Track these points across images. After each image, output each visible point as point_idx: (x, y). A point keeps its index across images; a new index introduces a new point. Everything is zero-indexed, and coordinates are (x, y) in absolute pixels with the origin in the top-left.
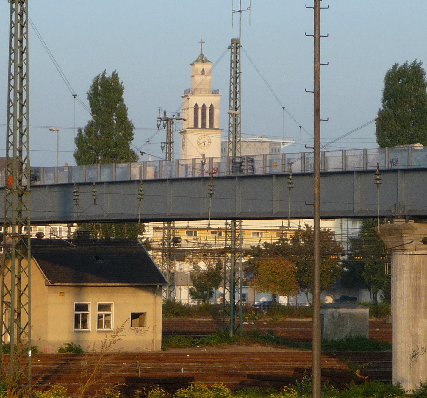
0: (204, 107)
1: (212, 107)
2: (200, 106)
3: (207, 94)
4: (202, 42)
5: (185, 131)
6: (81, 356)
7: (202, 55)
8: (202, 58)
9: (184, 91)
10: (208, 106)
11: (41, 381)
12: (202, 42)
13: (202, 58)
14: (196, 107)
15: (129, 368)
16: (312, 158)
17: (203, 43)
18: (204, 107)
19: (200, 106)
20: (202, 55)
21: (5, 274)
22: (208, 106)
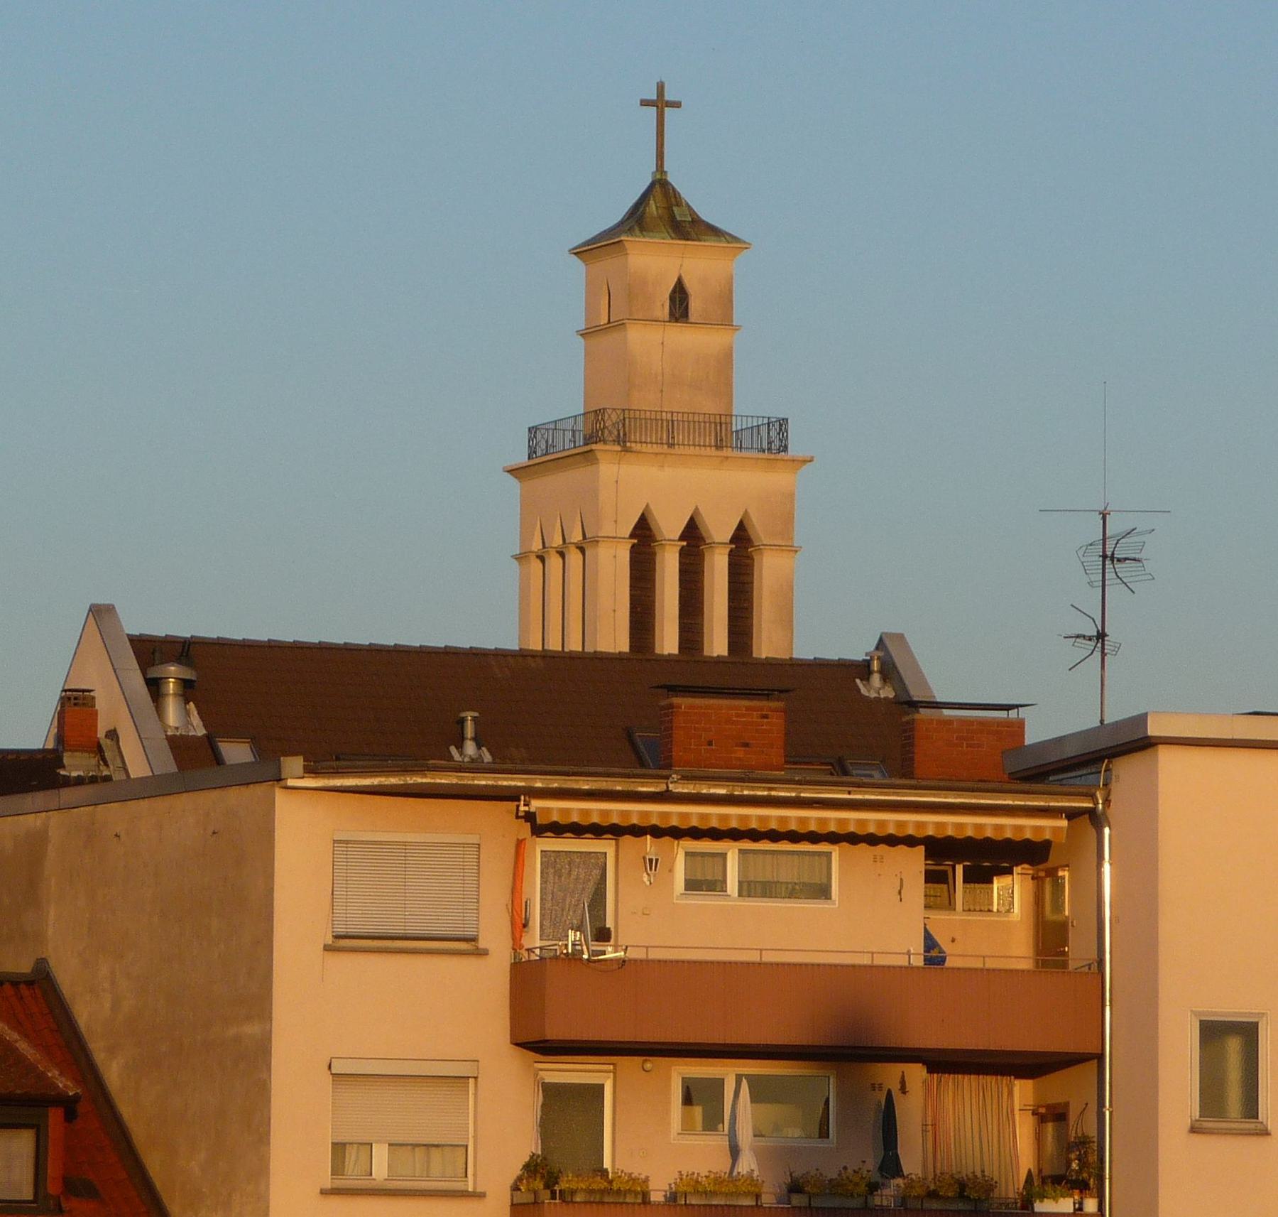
0: (693, 535)
1: (742, 539)
2: (670, 527)
3: (713, 452)
4: (660, 103)
5: (597, 541)
6: (939, 964)
7: (660, 187)
8: (669, 209)
9: (533, 430)
10: (720, 530)
11: (987, 866)
12: (660, 103)
13: (669, 209)
14: (643, 533)
15: (683, 201)
16: (984, 964)
17: (668, 111)
18: (693, 535)
19: (670, 527)
20: (660, 187)
21: (1193, 1015)
22: (720, 530)
